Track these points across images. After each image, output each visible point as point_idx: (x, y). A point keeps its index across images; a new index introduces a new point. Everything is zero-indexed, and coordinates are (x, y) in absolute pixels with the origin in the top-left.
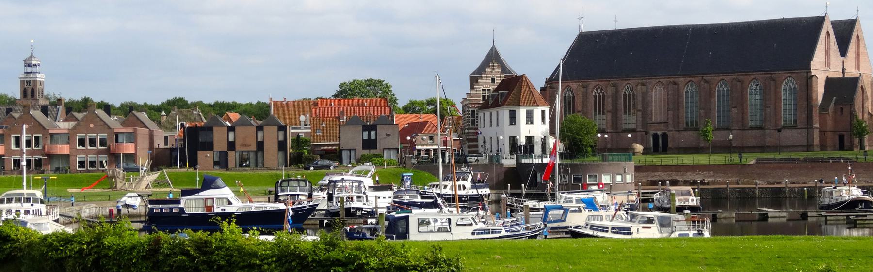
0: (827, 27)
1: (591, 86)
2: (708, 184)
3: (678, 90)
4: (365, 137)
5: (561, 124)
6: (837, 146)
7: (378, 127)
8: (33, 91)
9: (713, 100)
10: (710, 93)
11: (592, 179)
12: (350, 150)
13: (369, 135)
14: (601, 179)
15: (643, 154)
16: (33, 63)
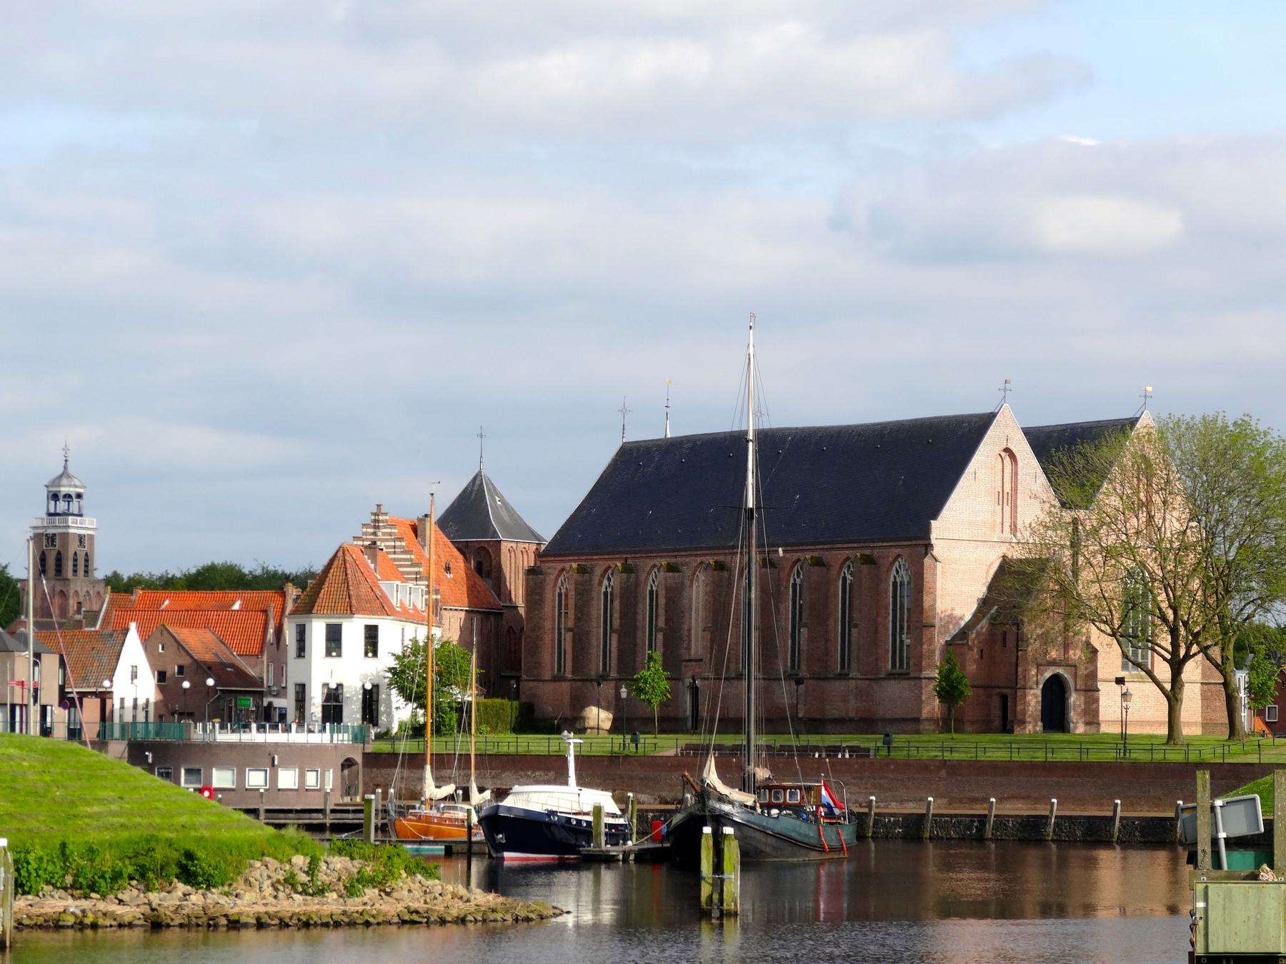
0: (1006, 433)
1: (598, 571)
2: (643, 803)
3: (637, 584)
6: (997, 723)
14: (209, 777)
15: (611, 731)
16: (64, 490)
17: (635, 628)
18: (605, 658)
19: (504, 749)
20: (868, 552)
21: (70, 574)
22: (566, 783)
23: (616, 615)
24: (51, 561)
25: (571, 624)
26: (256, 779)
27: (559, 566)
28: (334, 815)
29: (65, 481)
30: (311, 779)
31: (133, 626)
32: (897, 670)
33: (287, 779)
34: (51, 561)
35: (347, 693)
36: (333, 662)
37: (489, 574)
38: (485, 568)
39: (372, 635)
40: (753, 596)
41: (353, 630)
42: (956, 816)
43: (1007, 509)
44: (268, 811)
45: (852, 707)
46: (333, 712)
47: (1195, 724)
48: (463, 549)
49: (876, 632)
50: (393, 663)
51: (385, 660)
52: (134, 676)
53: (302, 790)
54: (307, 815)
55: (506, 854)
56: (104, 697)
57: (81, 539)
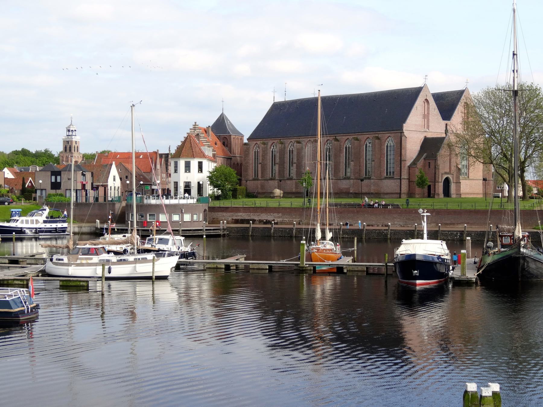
1: (270, 144)
3: (284, 148)
4: (53, 180)
5: (136, 172)
6: (426, 194)
7: (62, 172)
8: (70, 148)
9: (342, 155)
10: (340, 150)
11: (151, 217)
12: (42, 190)
13: (56, 179)
14: (158, 217)
16: (71, 129)
17: (284, 162)
18: (272, 172)
19: (258, 205)
20: (377, 135)
21: (73, 151)
22: (422, 238)
23: (278, 158)
24: (68, 148)
25: (260, 162)
26: (176, 218)
27: (255, 142)
28: (206, 232)
29: (71, 127)
30: (195, 217)
31: (114, 163)
32: (389, 176)
33: (187, 217)
34: (68, 148)
35: (192, 185)
36: (187, 174)
37: (227, 146)
38: (226, 143)
39: (200, 165)
40: (517, 137)
41: (194, 163)
42: (450, 231)
43: (426, 120)
44: (183, 230)
45: (373, 189)
46: (187, 190)
47: (481, 194)
48: (219, 137)
49: (380, 163)
50: (208, 174)
51: (206, 173)
52: (114, 180)
53: (192, 222)
54: (197, 232)
55: (418, 282)
56: (105, 187)
57: (76, 142)
